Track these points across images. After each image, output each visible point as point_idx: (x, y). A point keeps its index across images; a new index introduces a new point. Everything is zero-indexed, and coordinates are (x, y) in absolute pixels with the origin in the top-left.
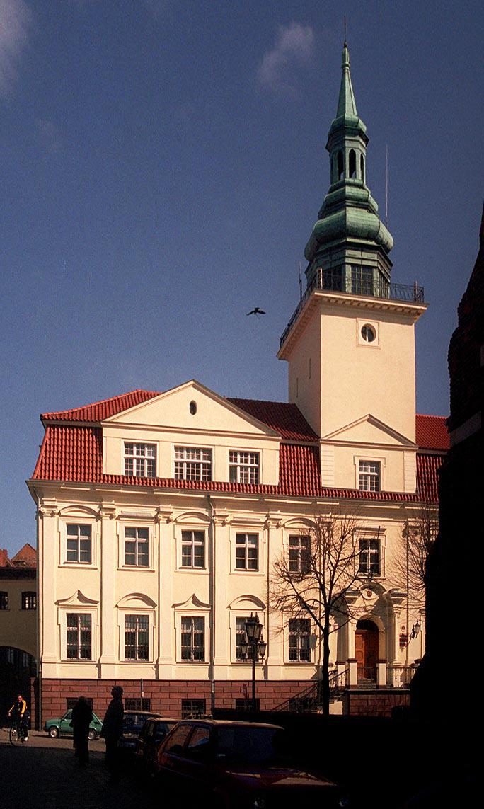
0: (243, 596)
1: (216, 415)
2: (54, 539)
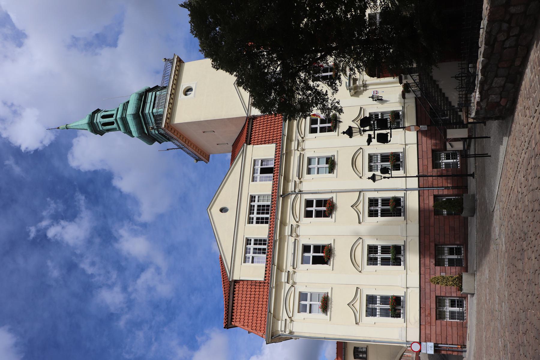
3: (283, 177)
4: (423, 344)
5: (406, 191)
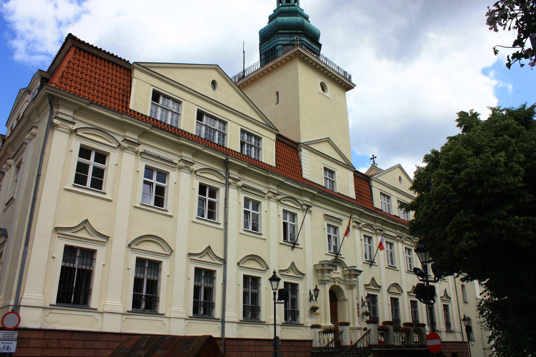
3: (316, 193)
4: (16, 335)
5: (222, 321)
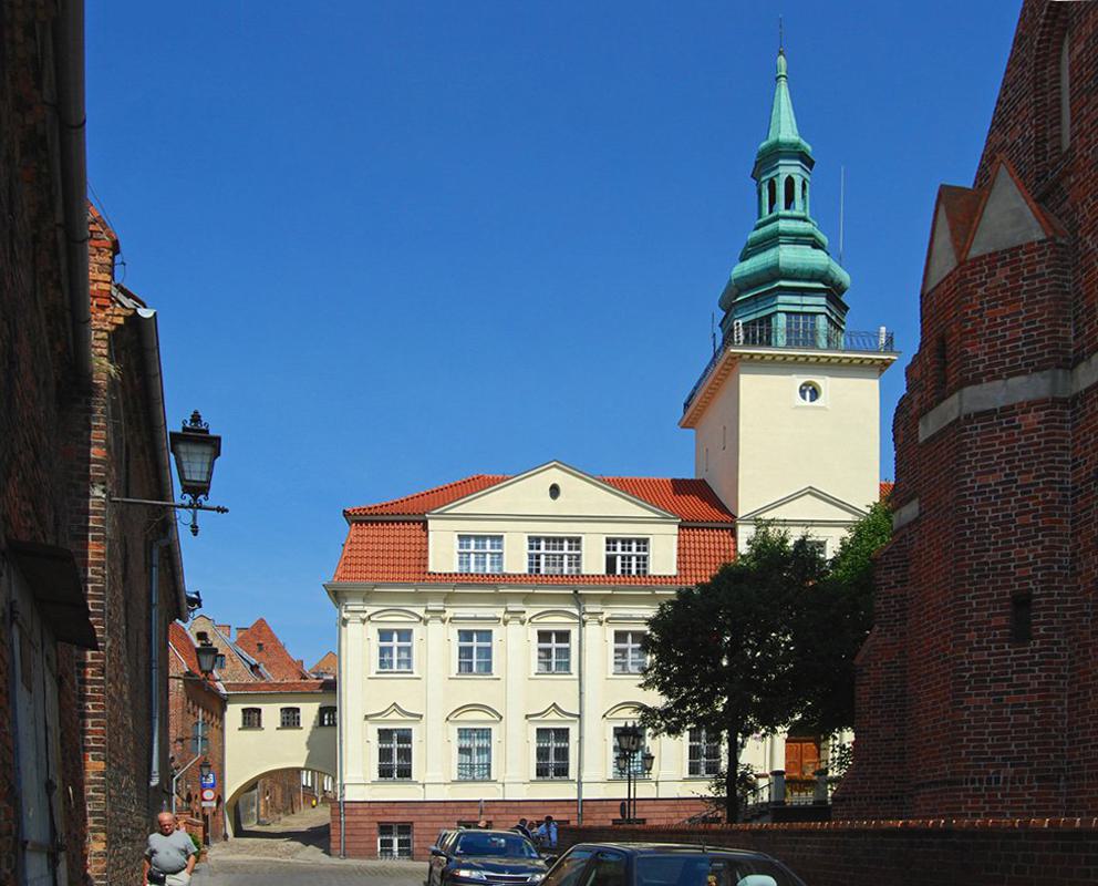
0: (456, 711)
1: (583, 496)
2: (359, 644)
3: (610, 592)
